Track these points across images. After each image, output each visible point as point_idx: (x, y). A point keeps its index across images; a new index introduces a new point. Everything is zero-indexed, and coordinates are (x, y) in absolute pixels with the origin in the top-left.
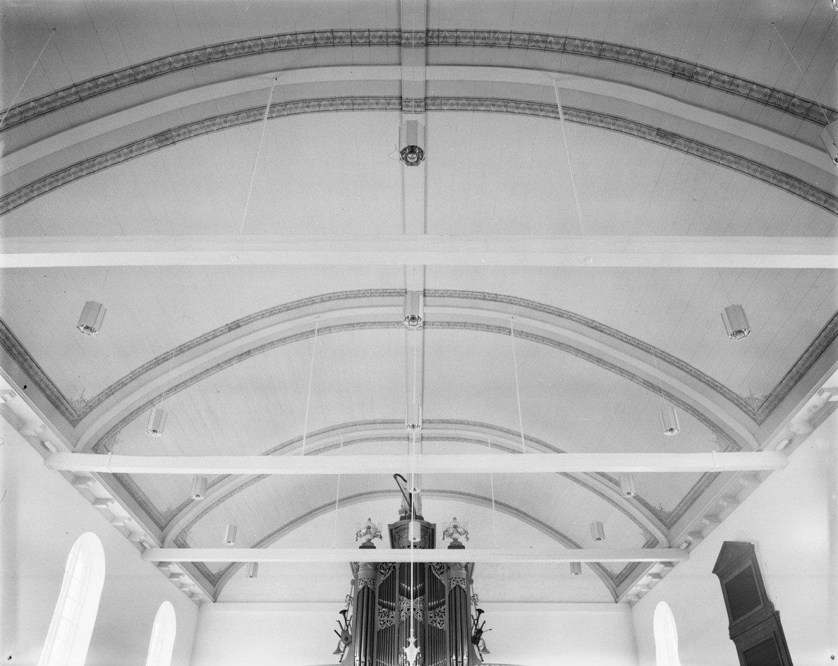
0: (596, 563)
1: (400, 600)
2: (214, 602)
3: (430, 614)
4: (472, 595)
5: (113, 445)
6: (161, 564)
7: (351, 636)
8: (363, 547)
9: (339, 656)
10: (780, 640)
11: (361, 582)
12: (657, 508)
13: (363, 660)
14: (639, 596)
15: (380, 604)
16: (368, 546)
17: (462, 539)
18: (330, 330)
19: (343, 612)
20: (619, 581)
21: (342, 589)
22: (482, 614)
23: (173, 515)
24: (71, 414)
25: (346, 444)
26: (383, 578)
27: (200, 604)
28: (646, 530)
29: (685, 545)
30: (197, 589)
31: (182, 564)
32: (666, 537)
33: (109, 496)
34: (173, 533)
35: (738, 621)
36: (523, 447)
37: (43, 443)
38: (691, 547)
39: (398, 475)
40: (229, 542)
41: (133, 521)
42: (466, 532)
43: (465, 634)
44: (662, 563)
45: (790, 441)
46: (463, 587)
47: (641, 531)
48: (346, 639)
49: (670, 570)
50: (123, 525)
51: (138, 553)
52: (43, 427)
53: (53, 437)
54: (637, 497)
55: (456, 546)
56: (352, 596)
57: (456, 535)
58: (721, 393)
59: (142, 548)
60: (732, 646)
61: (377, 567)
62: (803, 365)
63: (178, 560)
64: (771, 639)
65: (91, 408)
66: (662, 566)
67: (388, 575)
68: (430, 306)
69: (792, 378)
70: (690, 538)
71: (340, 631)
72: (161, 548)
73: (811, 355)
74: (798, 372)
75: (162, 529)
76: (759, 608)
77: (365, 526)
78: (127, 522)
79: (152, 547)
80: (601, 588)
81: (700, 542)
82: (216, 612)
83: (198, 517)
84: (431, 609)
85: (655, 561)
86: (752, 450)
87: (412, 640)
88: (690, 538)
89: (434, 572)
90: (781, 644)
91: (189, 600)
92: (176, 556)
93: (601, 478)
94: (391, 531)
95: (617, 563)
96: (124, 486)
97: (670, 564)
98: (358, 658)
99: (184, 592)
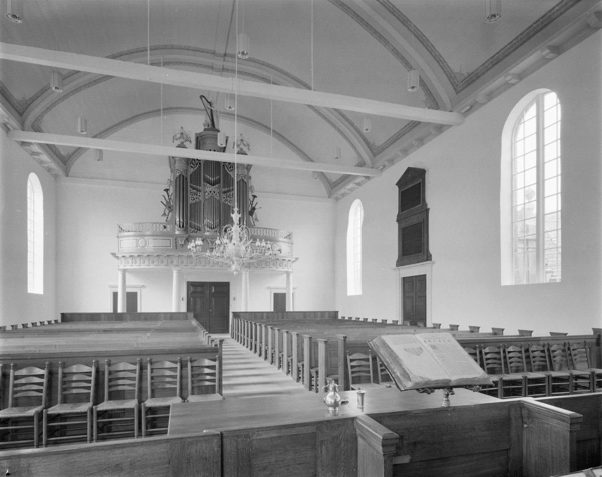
1: (204, 185)
2: (67, 176)
3: (224, 196)
4: (250, 186)
6: (23, 144)
7: (173, 206)
8: (179, 146)
9: (165, 218)
10: (426, 224)
11: (178, 171)
12: (372, 143)
13: (181, 220)
14: (343, 195)
15: (191, 187)
16: (181, 146)
17: (245, 149)
19: (167, 190)
20: (335, 186)
21: (165, 176)
22: (255, 198)
26: (192, 170)
27: (56, 176)
28: (359, 155)
29: (382, 167)
30: (53, 165)
32: (372, 161)
34: (30, 119)
35: (404, 212)
38: (385, 168)
39: (204, 97)
40: (83, 131)
43: (245, 209)
45: (471, 107)
46: (245, 180)
47: (356, 156)
48: (170, 208)
49: (367, 182)
55: (242, 152)
56: (172, 180)
57: (242, 146)
58: (441, 67)
60: (396, 225)
61: (189, 162)
67: (195, 169)
74: (498, 58)
75: (21, 114)
76: (419, 206)
77: (180, 132)
78: (49, 164)
79: (14, 129)
80: (322, 189)
82: (68, 183)
83: (49, 109)
85: (359, 173)
87: (236, 209)
88: (399, 153)
89: (226, 169)
90: (425, 226)
92: (35, 139)
94: (197, 138)
95: (335, 171)
97: (368, 178)
98: (178, 220)
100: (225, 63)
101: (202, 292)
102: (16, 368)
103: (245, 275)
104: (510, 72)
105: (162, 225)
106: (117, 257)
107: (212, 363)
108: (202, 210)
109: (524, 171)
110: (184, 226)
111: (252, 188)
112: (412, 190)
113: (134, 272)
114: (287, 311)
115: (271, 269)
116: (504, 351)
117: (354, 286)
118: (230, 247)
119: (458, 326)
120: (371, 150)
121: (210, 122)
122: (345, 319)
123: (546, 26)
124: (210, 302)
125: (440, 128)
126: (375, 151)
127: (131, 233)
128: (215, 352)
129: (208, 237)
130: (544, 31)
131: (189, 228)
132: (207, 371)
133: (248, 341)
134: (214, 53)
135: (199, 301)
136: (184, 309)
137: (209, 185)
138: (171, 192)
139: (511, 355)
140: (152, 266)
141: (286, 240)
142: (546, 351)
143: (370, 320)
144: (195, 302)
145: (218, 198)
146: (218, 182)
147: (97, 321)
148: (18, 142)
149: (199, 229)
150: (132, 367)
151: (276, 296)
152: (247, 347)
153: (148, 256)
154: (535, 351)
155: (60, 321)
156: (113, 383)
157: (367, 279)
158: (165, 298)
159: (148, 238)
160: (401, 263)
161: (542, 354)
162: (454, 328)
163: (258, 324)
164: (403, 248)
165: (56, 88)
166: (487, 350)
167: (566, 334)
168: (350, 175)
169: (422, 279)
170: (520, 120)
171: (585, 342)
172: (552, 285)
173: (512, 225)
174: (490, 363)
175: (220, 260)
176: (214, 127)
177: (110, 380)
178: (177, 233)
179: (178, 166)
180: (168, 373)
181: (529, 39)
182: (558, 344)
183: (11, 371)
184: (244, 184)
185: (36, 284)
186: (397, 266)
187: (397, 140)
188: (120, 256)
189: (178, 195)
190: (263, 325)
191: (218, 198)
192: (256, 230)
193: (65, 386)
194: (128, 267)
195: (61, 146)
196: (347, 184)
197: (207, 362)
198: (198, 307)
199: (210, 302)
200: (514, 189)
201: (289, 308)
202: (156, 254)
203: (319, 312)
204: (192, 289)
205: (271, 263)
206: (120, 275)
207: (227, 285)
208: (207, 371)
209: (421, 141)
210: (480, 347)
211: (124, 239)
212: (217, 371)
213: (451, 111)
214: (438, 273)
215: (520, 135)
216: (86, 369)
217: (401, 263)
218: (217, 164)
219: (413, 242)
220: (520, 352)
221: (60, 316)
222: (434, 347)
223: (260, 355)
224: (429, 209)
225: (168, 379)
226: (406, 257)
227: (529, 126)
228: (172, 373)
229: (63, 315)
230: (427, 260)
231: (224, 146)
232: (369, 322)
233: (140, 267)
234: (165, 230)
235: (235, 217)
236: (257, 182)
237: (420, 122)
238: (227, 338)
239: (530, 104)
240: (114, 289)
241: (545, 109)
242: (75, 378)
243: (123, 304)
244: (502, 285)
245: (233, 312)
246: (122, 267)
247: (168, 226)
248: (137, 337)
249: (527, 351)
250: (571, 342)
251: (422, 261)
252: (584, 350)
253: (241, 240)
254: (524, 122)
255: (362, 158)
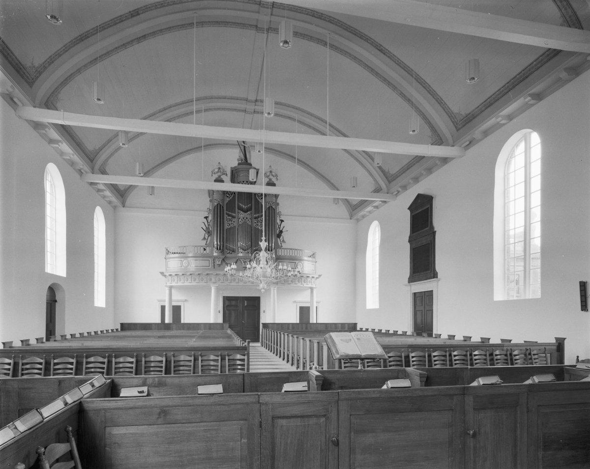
0: (346, 199)
5: (57, 102)
6: (92, 184)
8: (216, 181)
9: (205, 242)
10: (433, 245)
12: (387, 171)
13: (219, 244)
14: (363, 217)
15: (227, 214)
16: (219, 180)
17: (274, 180)
18: (203, 24)
19: (206, 218)
20: (354, 208)
21: (205, 205)
23: (98, 152)
24: (27, 77)
25: (206, 110)
26: (228, 199)
27: (115, 207)
29: (396, 192)
30: (114, 199)
31: (105, 184)
32: (387, 186)
33: (60, 139)
35: (414, 234)
36: (328, 132)
37: (12, 99)
40: (140, 174)
41: (75, 156)
42: (276, 176)
44: (381, 201)
45: (470, 142)
48: (209, 232)
50: (69, 158)
51: (78, 176)
52: (12, 87)
53: (18, 94)
54: (380, 168)
55: (271, 184)
58: (443, 108)
59: (80, 172)
60: (408, 245)
61: (225, 193)
62: (494, 99)
63: (103, 182)
64: (429, 244)
65: (40, 73)
66: (380, 202)
67: (231, 198)
68: (276, 16)
69: (485, 105)
70: (400, 189)
71: (205, 228)
72: (93, 173)
73: (500, 93)
75: (92, 161)
78: (72, 156)
79: (86, 172)
80: (343, 211)
81: (404, 192)
82: (124, 213)
84: (256, 218)
85: (377, 199)
86: (448, 145)
87: (263, 238)
88: (400, 189)
91: (109, 205)
92: (102, 180)
93: (364, 154)
95: (355, 198)
96: (67, 131)
97: (385, 202)
98: (216, 243)
99: (106, 200)
100: (256, 107)
101: (237, 306)
102: (116, 357)
103: (274, 291)
104: (501, 114)
105: (202, 248)
106: (165, 276)
107: (242, 357)
108: (236, 234)
109: (515, 200)
110: (221, 249)
111: (280, 214)
112: (422, 214)
113: (180, 288)
114: (311, 322)
115: (296, 285)
116: (471, 355)
117: (372, 300)
118: (259, 270)
119: (454, 336)
120: (386, 178)
121: (243, 157)
122: (390, 332)
123: (527, 77)
124: (243, 313)
125: (445, 160)
126: (390, 178)
127: (177, 255)
128: (244, 350)
129: (241, 257)
130: (527, 80)
131: (225, 250)
132: (238, 362)
133: (274, 348)
134: (247, 100)
135: (233, 313)
136: (220, 320)
137: (241, 212)
138: (210, 218)
139: (476, 357)
140: (194, 284)
141: (310, 259)
142: (508, 355)
143: (383, 331)
144: (230, 314)
145: (250, 223)
146: (249, 209)
147: (149, 330)
148: (88, 183)
149: (234, 251)
150: (188, 358)
151: (301, 308)
152: (274, 353)
153: (191, 274)
154: (498, 355)
155: (119, 330)
156: (176, 369)
157: (383, 294)
158: (204, 310)
159: (191, 259)
160: (412, 279)
161: (506, 358)
162: (451, 338)
163: (282, 333)
164: (414, 266)
165: (123, 144)
166: (455, 353)
167: (510, 341)
168: (367, 200)
169: (430, 294)
170: (511, 155)
171: (545, 348)
172: (536, 300)
173: (505, 247)
174: (458, 364)
175: (251, 279)
176: (247, 161)
177: (174, 367)
178: (215, 254)
179: (215, 196)
180: (212, 363)
181: (514, 87)
182: (521, 350)
183: (113, 359)
184: (273, 210)
185: (100, 300)
186: (409, 282)
187: (408, 169)
188: (167, 274)
189: (216, 222)
190: (286, 334)
191: (250, 223)
192: (283, 250)
193: (146, 370)
194: (174, 284)
195: (120, 185)
196: (366, 207)
197: (239, 357)
198: (233, 318)
199: (243, 313)
200: (506, 216)
201: (313, 320)
202: (197, 273)
203: (340, 323)
204: (227, 303)
205: (297, 281)
206: (167, 292)
207: (257, 299)
208: (238, 362)
209: (430, 171)
210: (450, 351)
211: (171, 260)
212: (246, 363)
213: (453, 146)
214: (444, 289)
215: (512, 168)
216: (159, 359)
217: (412, 279)
218: (249, 195)
219: (423, 262)
220: (486, 355)
221: (119, 325)
222: (358, 339)
223: (284, 359)
224: (436, 231)
225: (212, 368)
226: (416, 274)
227: (519, 160)
228: (215, 364)
229: (122, 324)
230: (434, 278)
231: (255, 180)
232: (383, 333)
233: (191, 284)
234: (205, 252)
235: (263, 244)
236: (284, 208)
237: (424, 157)
238: (258, 346)
239: (520, 141)
240: (162, 302)
241: (532, 146)
242: (152, 365)
243: (170, 314)
244: (495, 300)
245: (263, 324)
246: (169, 284)
247: (207, 249)
248: (186, 341)
249: (491, 355)
250: (513, 348)
251: (430, 279)
252: (544, 355)
253: (267, 264)
254: (515, 157)
255: (379, 184)
